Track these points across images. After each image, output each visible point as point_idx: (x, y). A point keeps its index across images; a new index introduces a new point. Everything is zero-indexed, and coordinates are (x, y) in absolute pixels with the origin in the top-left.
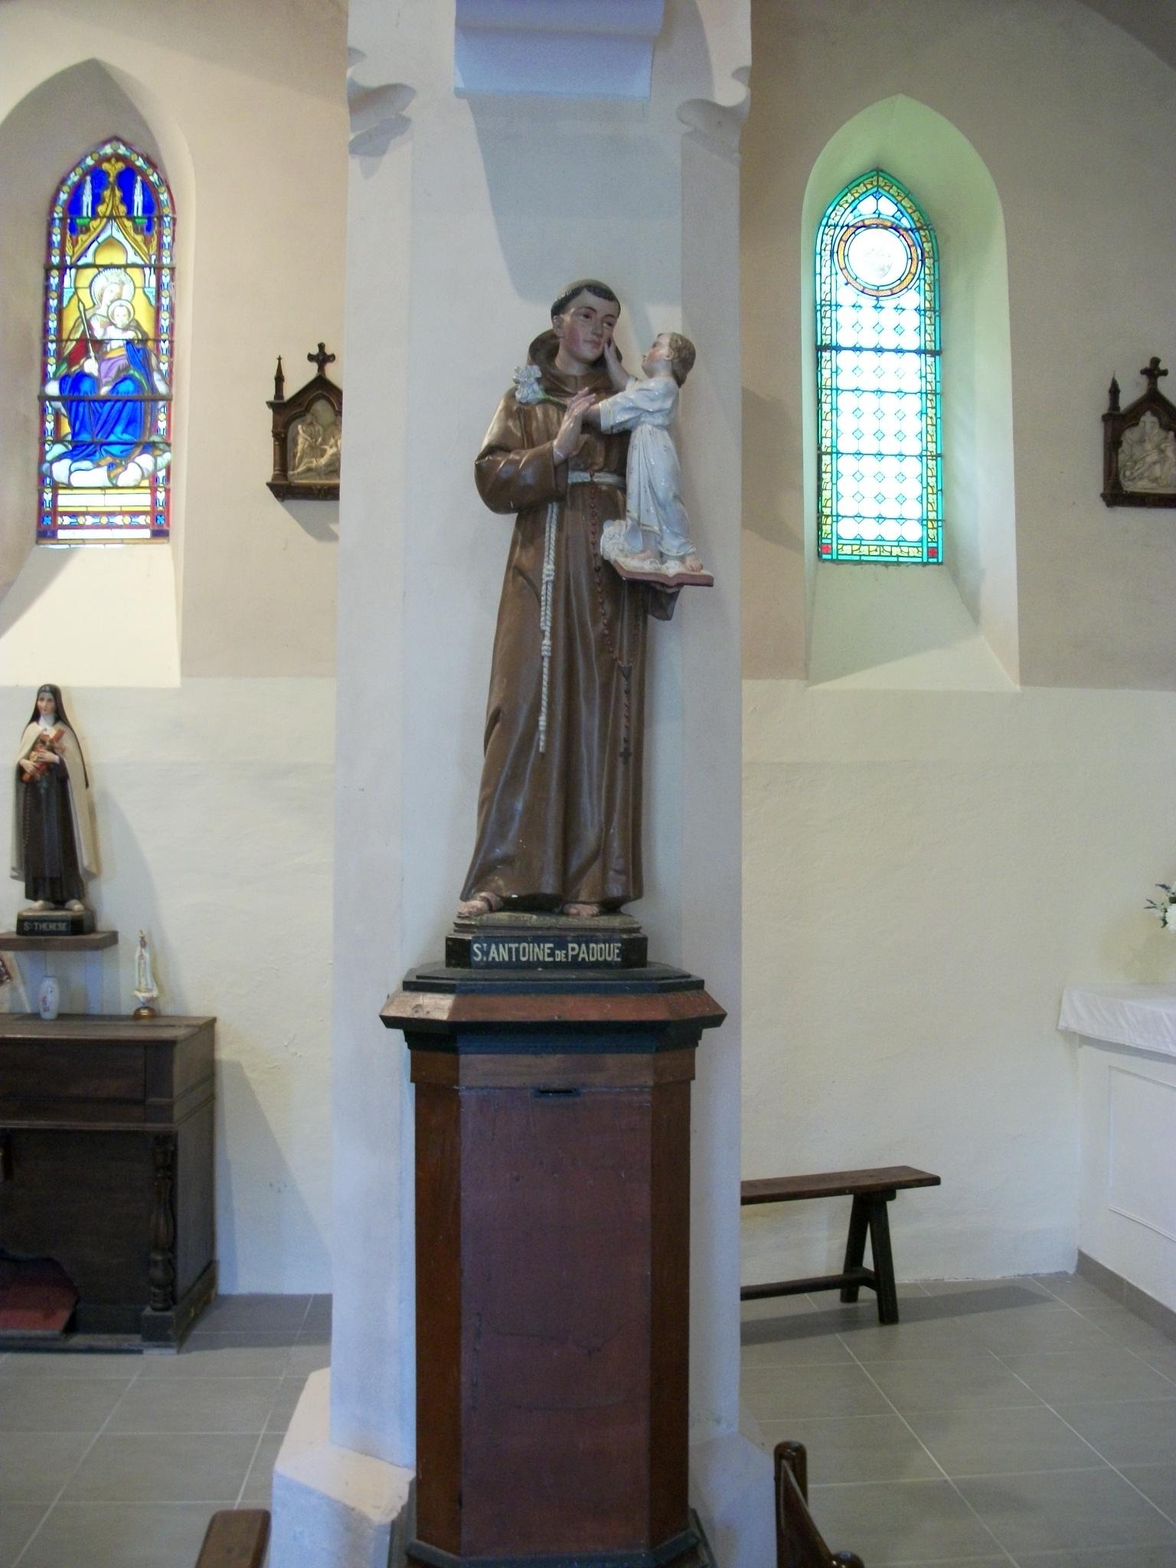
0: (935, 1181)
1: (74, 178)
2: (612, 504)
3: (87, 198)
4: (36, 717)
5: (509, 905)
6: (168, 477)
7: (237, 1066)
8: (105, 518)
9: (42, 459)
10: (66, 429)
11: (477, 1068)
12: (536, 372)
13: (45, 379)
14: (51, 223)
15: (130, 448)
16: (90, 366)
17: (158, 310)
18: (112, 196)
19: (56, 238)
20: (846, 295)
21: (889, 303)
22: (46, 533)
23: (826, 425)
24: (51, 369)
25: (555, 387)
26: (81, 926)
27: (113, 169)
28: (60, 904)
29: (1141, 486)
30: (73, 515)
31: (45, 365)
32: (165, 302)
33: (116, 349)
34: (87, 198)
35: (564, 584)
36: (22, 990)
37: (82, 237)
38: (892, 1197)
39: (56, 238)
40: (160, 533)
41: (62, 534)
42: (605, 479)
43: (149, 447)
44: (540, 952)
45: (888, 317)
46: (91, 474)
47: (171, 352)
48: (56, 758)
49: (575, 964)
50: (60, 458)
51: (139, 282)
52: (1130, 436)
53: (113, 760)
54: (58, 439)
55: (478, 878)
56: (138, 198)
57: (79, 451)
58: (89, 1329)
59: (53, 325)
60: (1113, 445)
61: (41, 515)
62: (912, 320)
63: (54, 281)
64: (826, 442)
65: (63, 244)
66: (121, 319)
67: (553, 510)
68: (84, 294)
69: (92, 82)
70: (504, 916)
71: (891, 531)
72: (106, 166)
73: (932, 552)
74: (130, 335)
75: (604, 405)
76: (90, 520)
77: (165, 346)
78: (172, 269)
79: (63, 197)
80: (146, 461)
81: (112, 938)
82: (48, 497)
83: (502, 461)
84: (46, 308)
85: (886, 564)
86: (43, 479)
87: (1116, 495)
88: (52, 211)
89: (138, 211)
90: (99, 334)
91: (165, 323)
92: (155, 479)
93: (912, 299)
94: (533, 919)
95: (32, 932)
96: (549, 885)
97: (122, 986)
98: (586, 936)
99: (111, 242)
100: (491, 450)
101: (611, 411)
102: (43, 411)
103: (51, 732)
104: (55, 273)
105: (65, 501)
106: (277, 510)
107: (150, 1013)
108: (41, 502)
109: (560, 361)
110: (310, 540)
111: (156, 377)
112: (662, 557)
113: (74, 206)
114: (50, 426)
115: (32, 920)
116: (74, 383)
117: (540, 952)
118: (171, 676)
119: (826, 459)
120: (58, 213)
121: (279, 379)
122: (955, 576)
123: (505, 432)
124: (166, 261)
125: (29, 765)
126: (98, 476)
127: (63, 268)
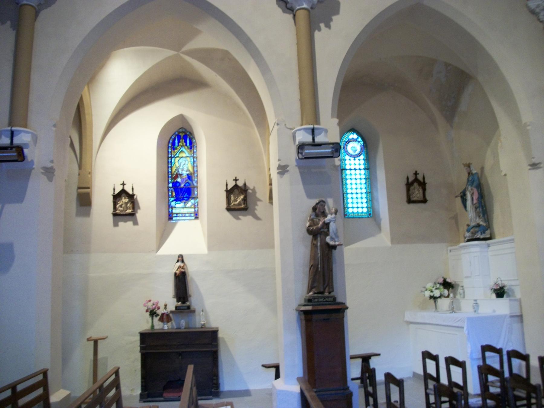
1: (173, 137)
2: (327, 234)
3: (176, 141)
4: (178, 261)
5: (315, 293)
6: (198, 205)
7: (223, 338)
8: (184, 215)
9: (169, 202)
10: (174, 194)
11: (315, 317)
12: (314, 213)
13: (169, 183)
14: (168, 147)
15: (188, 199)
16: (179, 180)
17: (194, 167)
18: (182, 141)
19: (170, 151)
20: (347, 157)
21: (357, 159)
22: (170, 217)
23: (344, 187)
24: (170, 181)
25: (317, 216)
26: (189, 307)
27: (182, 135)
28: (184, 302)
29: (415, 199)
30: (177, 214)
32: (195, 165)
33: (185, 176)
34: (176, 141)
35: (321, 245)
37: (176, 151)
39: (170, 151)
40: (197, 218)
41: (174, 219)
42: (326, 230)
43: (193, 198)
44: (322, 300)
45: (357, 161)
46: (180, 205)
47: (197, 176)
48: (183, 270)
49: (327, 301)
51: (189, 160)
52: (412, 188)
53: (192, 269)
54: (172, 197)
55: (310, 289)
57: (176, 200)
59: (170, 171)
60: (408, 190)
61: (169, 215)
62: (362, 162)
63: (170, 161)
64: (345, 191)
66: (185, 169)
67: (319, 236)
69: (181, 118)
70: (316, 295)
71: (360, 210)
72: (180, 134)
73: (370, 214)
74: (188, 173)
75: (326, 219)
78: (197, 158)
79: (171, 141)
81: (194, 311)
82: (170, 210)
83: (311, 228)
84: (168, 167)
85: (360, 218)
86: (170, 206)
87: (410, 201)
89: (188, 144)
90: (180, 172)
93: (362, 157)
94: (320, 295)
96: (322, 290)
97: (200, 321)
98: (328, 297)
99: (182, 151)
100: (309, 226)
101: (327, 220)
102: (169, 190)
103: (182, 265)
104: (170, 159)
105: (174, 211)
106: (227, 214)
107: (203, 326)
108: (169, 211)
109: (317, 211)
111: (194, 182)
112: (335, 242)
114: (170, 194)
115: (179, 307)
116: (176, 185)
117: (322, 300)
118: (206, 251)
119: (345, 195)
120: (170, 145)
122: (375, 220)
123: (310, 223)
124: (195, 155)
125: (178, 272)
127: (172, 158)
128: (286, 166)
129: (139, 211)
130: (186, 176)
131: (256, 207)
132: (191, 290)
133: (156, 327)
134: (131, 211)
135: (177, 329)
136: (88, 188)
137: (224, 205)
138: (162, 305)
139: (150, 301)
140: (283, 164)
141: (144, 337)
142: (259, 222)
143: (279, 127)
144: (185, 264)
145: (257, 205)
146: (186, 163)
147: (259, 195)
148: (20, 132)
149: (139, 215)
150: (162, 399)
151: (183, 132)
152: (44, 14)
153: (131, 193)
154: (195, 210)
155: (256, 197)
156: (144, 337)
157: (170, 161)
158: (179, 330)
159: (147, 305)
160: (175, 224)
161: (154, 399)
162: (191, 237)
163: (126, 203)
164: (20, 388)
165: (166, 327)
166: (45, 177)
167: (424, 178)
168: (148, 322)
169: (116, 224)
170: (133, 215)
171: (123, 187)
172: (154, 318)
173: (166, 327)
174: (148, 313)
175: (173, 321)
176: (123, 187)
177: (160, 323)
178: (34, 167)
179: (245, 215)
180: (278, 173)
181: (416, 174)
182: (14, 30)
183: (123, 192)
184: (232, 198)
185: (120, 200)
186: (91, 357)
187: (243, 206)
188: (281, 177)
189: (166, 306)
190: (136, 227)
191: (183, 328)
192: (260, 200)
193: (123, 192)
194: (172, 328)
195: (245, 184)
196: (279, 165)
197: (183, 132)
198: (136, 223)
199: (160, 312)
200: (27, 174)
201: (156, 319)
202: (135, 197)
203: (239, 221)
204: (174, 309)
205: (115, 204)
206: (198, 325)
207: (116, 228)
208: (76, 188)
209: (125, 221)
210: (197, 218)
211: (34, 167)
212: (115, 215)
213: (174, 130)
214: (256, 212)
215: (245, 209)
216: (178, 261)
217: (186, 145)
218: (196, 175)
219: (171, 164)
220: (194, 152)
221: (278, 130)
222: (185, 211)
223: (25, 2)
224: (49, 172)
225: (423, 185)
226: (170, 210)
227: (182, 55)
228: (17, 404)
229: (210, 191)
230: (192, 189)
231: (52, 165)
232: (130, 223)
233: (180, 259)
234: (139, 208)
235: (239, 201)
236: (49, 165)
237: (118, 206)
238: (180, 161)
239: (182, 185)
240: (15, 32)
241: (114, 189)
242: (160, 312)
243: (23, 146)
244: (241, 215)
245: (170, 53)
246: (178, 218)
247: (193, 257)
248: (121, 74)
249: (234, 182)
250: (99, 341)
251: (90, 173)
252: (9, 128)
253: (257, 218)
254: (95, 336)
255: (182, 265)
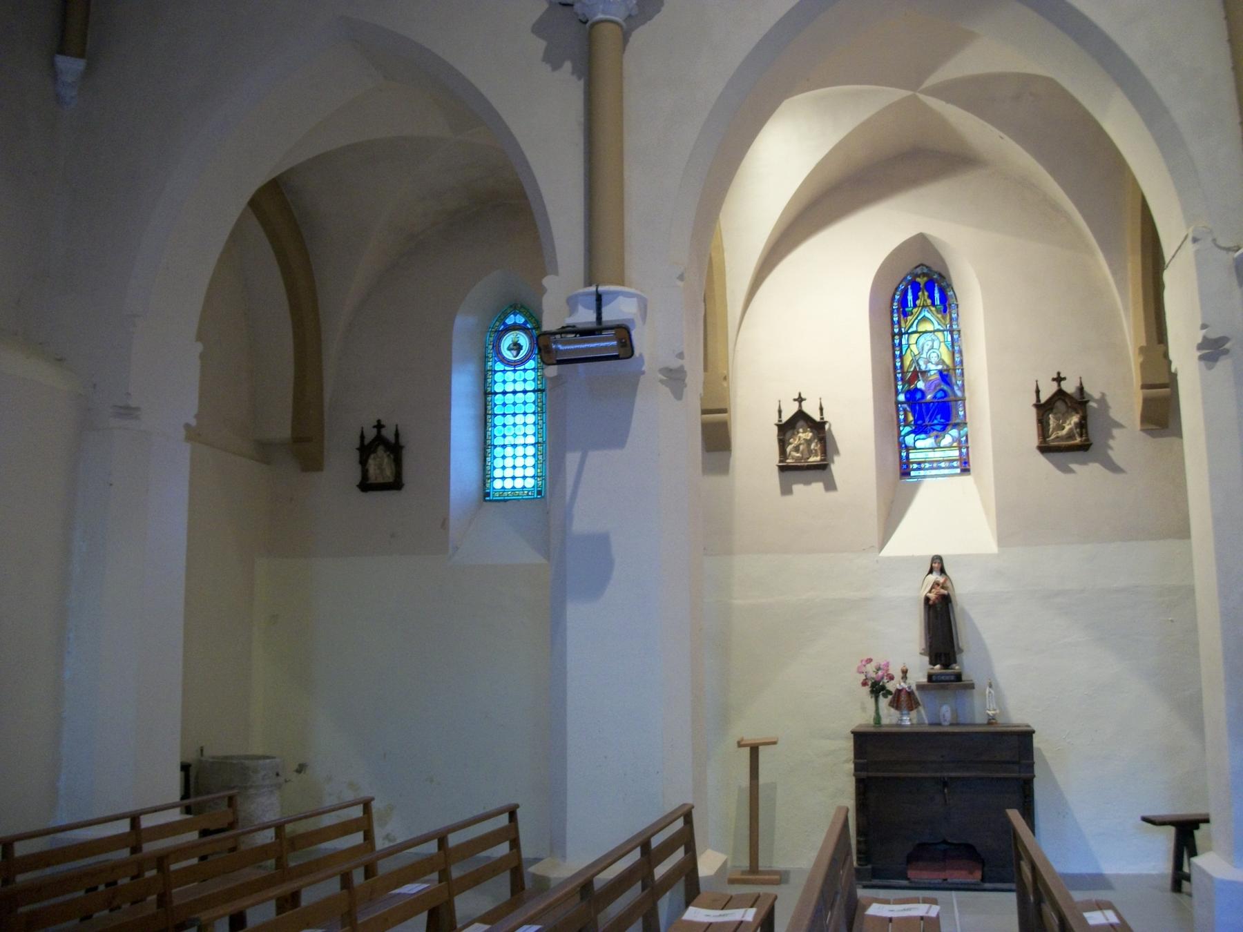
0: (1145, 819)
3: (910, 297)
4: (931, 572)
6: (967, 441)
8: (935, 464)
9: (899, 436)
10: (911, 418)
13: (897, 393)
14: (892, 312)
15: (944, 428)
16: (921, 385)
18: (923, 296)
19: (896, 319)
22: (905, 473)
24: (900, 387)
26: (958, 677)
27: (922, 281)
30: (919, 463)
31: (896, 386)
33: (933, 375)
34: (910, 297)
36: (923, 712)
38: (1197, 828)
39: (896, 319)
40: (965, 470)
41: (913, 473)
43: (955, 426)
46: (925, 442)
47: (962, 374)
48: (945, 592)
50: (908, 434)
51: (942, 339)
53: (963, 589)
54: (907, 424)
56: (937, 296)
57: (920, 429)
58: (991, 880)
59: (898, 364)
63: (897, 342)
65: (899, 322)
66: (934, 359)
68: (913, 347)
69: (921, 242)
72: (918, 280)
74: (940, 367)
76: (927, 465)
77: (958, 372)
80: (954, 432)
82: (904, 454)
84: (894, 356)
86: (903, 446)
88: (892, 305)
89: (937, 302)
91: (957, 360)
92: (960, 442)
95: (936, 681)
99: (925, 319)
102: (898, 411)
103: (941, 579)
106: (1041, 460)
107: (991, 721)
108: (901, 457)
110: (1058, 473)
113: (903, 302)
115: (937, 675)
116: (912, 395)
121: (1038, 392)
125: (932, 596)
126: (930, 442)
127: (901, 334)
128: (1223, 340)
129: (836, 458)
130: (937, 376)
131: (1111, 442)
132: (964, 636)
133: (885, 721)
134: (818, 458)
135: (931, 724)
136: (724, 411)
137: (1033, 439)
138: (896, 671)
139: (869, 661)
140: (1213, 336)
141: (865, 741)
142: (1119, 477)
143: (1197, 246)
144: (948, 578)
145: (1113, 437)
146: (936, 345)
147: (1115, 414)
148: (616, 294)
149: (838, 467)
150: (904, 883)
151: (924, 275)
152: (639, 36)
153: (817, 418)
154: (961, 453)
155: (1110, 418)
156: (865, 741)
157: (897, 342)
158: (991, 729)
159: (863, 669)
160: (916, 487)
161: (885, 882)
162: (955, 516)
163: (808, 442)
164: (656, 842)
165: (908, 720)
166: (667, 390)
167: (397, 435)
168: (864, 709)
169: (786, 490)
170: (823, 467)
171: (379, 432)
172: (881, 697)
173: (906, 721)
174: (867, 689)
175: (921, 708)
176: (379, 432)
177: (893, 710)
178: (644, 368)
179: (1084, 463)
180: (1201, 358)
181: (379, 426)
182: (580, 78)
183: (801, 417)
184: (1052, 421)
185: (793, 435)
186: (745, 781)
187: (1078, 440)
188: (1210, 368)
189: (905, 672)
190: (832, 494)
191: (947, 723)
192: (1119, 426)
193: (801, 417)
194: (920, 724)
195: (1081, 389)
196: (1205, 338)
197: (924, 275)
198: (830, 486)
199: (892, 686)
200: (631, 384)
201: (884, 702)
202: (827, 427)
203: (1070, 476)
204: (924, 680)
205: (783, 444)
206: (980, 719)
207: (788, 498)
208: (699, 412)
209: (808, 483)
210: (965, 467)
211: (644, 368)
212: (783, 469)
213: (904, 269)
214: (1110, 452)
215: (1085, 447)
216: (931, 572)
217: (933, 304)
218: (958, 372)
219: (901, 351)
220: (951, 319)
221: (1197, 253)
222: (938, 455)
223: (600, 16)
224: (675, 378)
225: (395, 450)
226: (904, 454)
227: (921, 96)
228: (652, 875)
229: (996, 407)
230: (953, 404)
231: (680, 362)
232: (818, 487)
233: (935, 565)
234: (837, 452)
235: (1067, 428)
236: (674, 363)
237: (789, 449)
238: (922, 340)
239: (929, 397)
240: (582, 83)
241: (780, 412)
242: (892, 686)
243: (629, 325)
244: (1072, 462)
245: (899, 94)
246: (922, 473)
247: (966, 560)
248: (785, 155)
249: (1055, 384)
250: (761, 748)
251: (725, 378)
252: (593, 289)
253: (1114, 468)
254: (752, 737)
255: (941, 579)
